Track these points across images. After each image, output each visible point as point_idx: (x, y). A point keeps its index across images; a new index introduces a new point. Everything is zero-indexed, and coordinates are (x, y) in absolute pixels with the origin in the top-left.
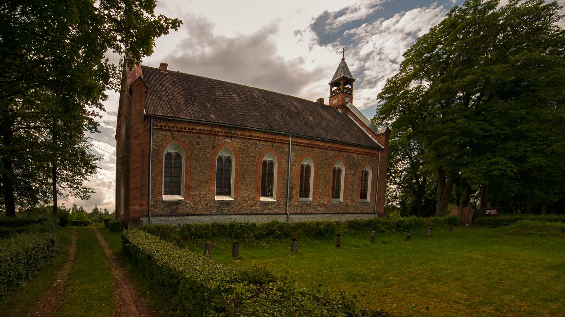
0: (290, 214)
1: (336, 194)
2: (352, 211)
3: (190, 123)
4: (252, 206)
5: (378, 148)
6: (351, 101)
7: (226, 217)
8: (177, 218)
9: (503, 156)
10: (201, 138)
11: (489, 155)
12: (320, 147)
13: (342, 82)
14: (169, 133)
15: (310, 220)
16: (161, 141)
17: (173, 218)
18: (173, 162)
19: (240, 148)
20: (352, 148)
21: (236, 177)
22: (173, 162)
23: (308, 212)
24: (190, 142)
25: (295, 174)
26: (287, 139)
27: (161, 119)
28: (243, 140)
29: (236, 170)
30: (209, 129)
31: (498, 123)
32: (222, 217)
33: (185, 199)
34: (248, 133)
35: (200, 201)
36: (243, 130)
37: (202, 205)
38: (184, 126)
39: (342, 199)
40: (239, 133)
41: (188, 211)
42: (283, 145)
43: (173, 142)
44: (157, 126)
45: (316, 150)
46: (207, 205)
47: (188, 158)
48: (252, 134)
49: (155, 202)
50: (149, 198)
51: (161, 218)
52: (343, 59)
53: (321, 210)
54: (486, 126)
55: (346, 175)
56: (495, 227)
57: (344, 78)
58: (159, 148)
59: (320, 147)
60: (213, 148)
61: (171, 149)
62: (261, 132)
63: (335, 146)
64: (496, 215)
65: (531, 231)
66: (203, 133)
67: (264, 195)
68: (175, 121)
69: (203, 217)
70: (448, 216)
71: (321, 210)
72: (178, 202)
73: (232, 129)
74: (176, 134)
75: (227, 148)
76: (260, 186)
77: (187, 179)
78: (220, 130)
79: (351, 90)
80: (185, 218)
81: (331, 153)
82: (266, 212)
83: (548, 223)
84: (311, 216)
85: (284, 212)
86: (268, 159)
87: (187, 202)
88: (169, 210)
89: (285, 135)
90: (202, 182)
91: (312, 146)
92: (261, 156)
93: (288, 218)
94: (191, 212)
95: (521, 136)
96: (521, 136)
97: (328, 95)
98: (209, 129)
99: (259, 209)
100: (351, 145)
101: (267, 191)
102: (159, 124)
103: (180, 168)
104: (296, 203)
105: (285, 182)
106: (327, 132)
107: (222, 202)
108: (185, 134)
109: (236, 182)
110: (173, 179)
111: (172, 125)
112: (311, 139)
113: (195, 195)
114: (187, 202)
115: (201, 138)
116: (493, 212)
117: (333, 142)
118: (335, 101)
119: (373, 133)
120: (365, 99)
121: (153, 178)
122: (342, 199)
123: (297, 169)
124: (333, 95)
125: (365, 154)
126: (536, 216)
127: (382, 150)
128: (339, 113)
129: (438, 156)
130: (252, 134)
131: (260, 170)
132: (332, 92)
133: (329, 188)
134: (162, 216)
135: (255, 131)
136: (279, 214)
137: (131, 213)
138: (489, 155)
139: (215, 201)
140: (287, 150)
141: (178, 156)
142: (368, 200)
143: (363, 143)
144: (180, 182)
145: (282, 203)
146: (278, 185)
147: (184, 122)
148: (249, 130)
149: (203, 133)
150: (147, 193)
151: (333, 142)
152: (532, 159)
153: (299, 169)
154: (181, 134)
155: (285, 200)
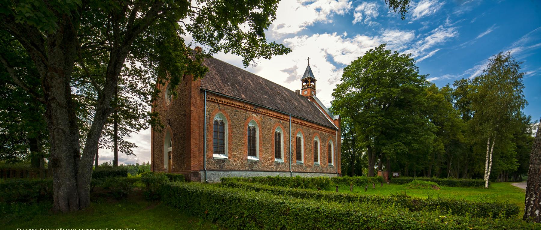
0: (210, 170)
1: (316, 160)
2: (325, 172)
3: (231, 99)
4: (270, 165)
5: (335, 129)
6: (315, 94)
7: (256, 173)
8: (225, 173)
9: (400, 141)
10: (237, 111)
11: (394, 140)
12: (306, 126)
13: (309, 80)
14: (216, 105)
15: (316, 177)
16: (212, 110)
17: (222, 173)
18: (219, 127)
19: (262, 121)
20: (323, 128)
21: (260, 143)
22: (219, 127)
23: (302, 171)
24: (231, 114)
25: (293, 143)
26: (288, 118)
27: (212, 93)
28: (263, 116)
29: (284, 141)
30: (243, 105)
31: (397, 121)
32: (253, 173)
33: (229, 158)
34: (266, 111)
35: (238, 160)
36: (263, 108)
37: (240, 163)
38: (227, 101)
39: (319, 162)
40: (261, 110)
41: (230, 167)
42: (286, 122)
43: (220, 112)
44: (209, 98)
45: (304, 127)
46: (242, 163)
47: (229, 126)
48: (269, 112)
49: (208, 159)
50: (204, 156)
51: (213, 172)
52: (309, 65)
53: (309, 169)
54: (391, 122)
55: (321, 146)
56: (401, 184)
57: (310, 78)
58: (211, 115)
59: (306, 126)
60: (245, 119)
61: (217, 118)
62: (274, 111)
63: (314, 125)
64: (398, 177)
65: (420, 186)
66: (238, 107)
67: (216, 152)
68: (221, 97)
69: (241, 173)
70: (378, 177)
71: (309, 169)
72: (224, 160)
73: (257, 107)
74: (221, 106)
75: (254, 120)
76: (274, 150)
77: (229, 142)
78: (249, 107)
79: (314, 86)
80: (230, 172)
81: (312, 130)
82: (278, 170)
83: (426, 182)
84: (304, 174)
85: (288, 170)
86: (277, 131)
87: (230, 160)
88: (218, 166)
89: (287, 115)
90: (239, 145)
91: (302, 125)
92: (274, 129)
93: (291, 175)
94: (232, 168)
95: (408, 131)
96: (408, 131)
97: (301, 88)
98: (243, 105)
99: (275, 167)
100: (322, 126)
101: (278, 155)
102: (210, 97)
103: (224, 133)
104: (295, 164)
105: (288, 149)
106: (308, 115)
107: (252, 161)
108: (227, 107)
109: (260, 147)
110: (219, 141)
111: (219, 99)
112: (301, 119)
113: (235, 155)
114: (230, 160)
115: (237, 111)
116: (396, 175)
117: (312, 122)
118: (306, 93)
119: (331, 118)
120: (325, 96)
121: (207, 139)
122: (319, 162)
123: (294, 140)
124: (304, 88)
125: (329, 132)
126: (421, 178)
127: (338, 130)
128: (308, 101)
129: (503, 172)
130: (269, 112)
131: (274, 139)
132: (303, 86)
133: (312, 155)
134: (213, 170)
135: (270, 110)
136: (286, 172)
137: (192, 168)
138: (394, 140)
139: (247, 160)
140: (288, 126)
141: (223, 124)
142: (333, 164)
143: (328, 125)
144: (224, 144)
145: (287, 164)
146: (284, 150)
147: (227, 98)
148: (267, 109)
149: (238, 107)
150: (203, 151)
151: (312, 122)
152: (414, 144)
153: (295, 140)
154: (225, 107)
155: (288, 162)
